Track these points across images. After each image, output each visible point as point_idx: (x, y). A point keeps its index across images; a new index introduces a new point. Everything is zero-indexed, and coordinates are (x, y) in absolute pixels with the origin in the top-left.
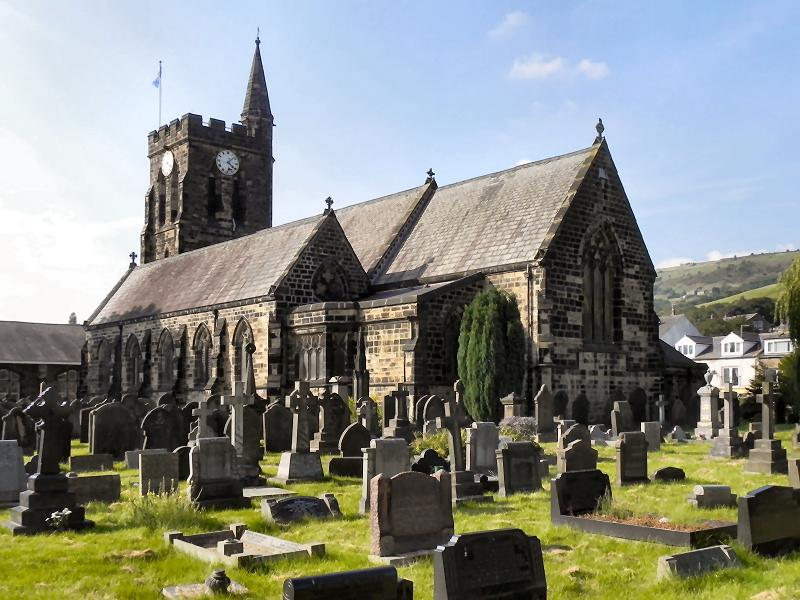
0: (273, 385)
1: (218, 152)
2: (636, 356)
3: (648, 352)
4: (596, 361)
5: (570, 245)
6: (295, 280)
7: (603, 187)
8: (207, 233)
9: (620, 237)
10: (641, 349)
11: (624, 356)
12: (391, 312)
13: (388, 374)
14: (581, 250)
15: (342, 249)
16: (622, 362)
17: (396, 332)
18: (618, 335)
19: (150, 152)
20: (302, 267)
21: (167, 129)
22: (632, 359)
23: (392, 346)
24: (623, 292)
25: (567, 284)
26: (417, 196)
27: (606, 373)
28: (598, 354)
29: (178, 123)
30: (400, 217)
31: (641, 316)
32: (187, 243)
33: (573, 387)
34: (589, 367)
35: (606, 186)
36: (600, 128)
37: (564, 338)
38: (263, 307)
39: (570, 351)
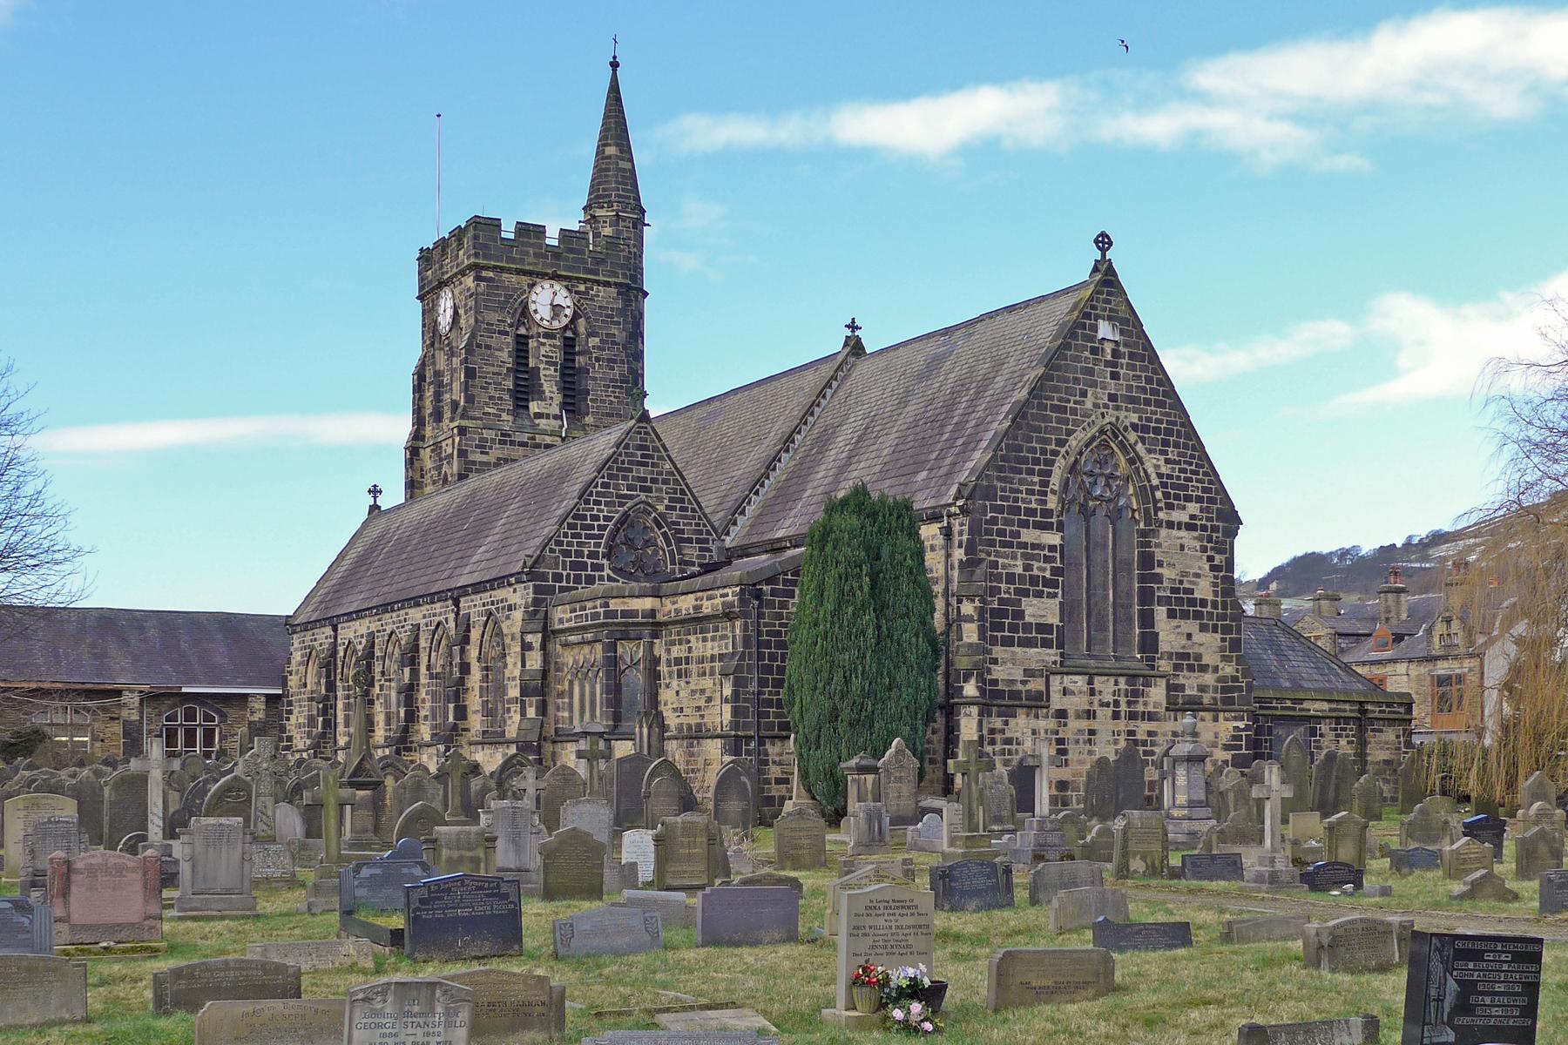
1: (532, 286)
2: (1190, 683)
3: (1221, 673)
4: (1092, 692)
6: (569, 544)
7: (1109, 357)
8: (512, 443)
9: (1149, 451)
10: (1204, 668)
11: (1163, 683)
12: (706, 603)
14: (1055, 481)
15: (665, 482)
16: (1157, 694)
17: (713, 639)
18: (1150, 643)
19: (421, 288)
20: (584, 518)
21: (442, 244)
22: (1182, 687)
24: (1158, 557)
25: (1024, 545)
26: (826, 371)
27: (1116, 716)
28: (1097, 679)
29: (458, 233)
31: (1203, 603)
32: (474, 463)
35: (1115, 353)
36: (1103, 242)
37: (1016, 649)
38: (518, 593)
39: (1029, 673)
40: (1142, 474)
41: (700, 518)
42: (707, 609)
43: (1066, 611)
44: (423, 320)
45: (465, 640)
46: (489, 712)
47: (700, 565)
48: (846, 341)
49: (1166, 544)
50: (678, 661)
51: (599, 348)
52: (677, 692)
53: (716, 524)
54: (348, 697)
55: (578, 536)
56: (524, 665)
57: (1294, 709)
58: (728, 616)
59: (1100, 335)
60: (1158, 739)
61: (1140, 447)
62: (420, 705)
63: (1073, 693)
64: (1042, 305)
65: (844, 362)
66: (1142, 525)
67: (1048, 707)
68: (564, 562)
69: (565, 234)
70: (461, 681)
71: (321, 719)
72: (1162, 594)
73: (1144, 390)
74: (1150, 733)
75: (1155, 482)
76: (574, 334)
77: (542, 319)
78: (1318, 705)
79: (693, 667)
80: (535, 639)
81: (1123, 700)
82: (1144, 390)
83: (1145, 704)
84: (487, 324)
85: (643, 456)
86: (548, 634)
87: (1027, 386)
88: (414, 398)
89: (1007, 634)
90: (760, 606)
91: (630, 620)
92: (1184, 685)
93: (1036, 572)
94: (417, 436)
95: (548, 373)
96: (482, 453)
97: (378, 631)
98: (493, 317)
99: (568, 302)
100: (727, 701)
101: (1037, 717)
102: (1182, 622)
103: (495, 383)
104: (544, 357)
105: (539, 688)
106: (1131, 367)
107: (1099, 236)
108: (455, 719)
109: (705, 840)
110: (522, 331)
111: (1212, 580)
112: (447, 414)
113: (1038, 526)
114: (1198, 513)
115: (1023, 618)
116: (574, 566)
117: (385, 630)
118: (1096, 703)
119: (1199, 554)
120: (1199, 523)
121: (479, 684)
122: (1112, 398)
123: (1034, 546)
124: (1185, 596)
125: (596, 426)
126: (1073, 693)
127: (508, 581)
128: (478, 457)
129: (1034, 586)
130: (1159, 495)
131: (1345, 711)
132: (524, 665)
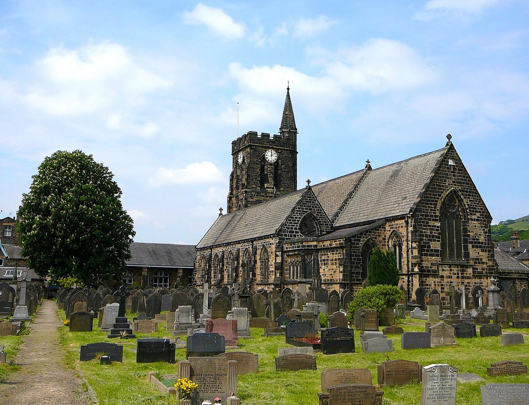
0: (276, 282)
2: (479, 267)
3: (488, 264)
5: (431, 204)
6: (289, 225)
8: (260, 196)
9: (465, 198)
10: (483, 263)
12: (333, 243)
13: (333, 277)
16: (470, 271)
17: (336, 254)
18: (467, 255)
21: (240, 139)
23: (334, 262)
25: (430, 226)
26: (360, 175)
27: (458, 277)
30: (351, 188)
31: (482, 243)
32: (249, 201)
33: (435, 285)
34: (446, 273)
35: (454, 169)
36: (449, 137)
37: (429, 257)
40: (463, 204)
41: (326, 218)
42: (334, 246)
43: (443, 245)
44: (233, 160)
45: (256, 253)
46: (263, 274)
47: (326, 232)
48: (366, 166)
50: (324, 260)
51: (284, 168)
52: (324, 270)
53: (330, 219)
54: (215, 270)
55: (292, 223)
56: (276, 261)
58: (342, 247)
59: (450, 164)
60: (471, 285)
62: (240, 272)
64: (430, 155)
65: (366, 172)
66: (463, 220)
67: (438, 275)
68: (287, 231)
69: (275, 136)
70: (254, 266)
71: (207, 276)
73: (462, 180)
74: (468, 283)
75: (467, 207)
76: (277, 164)
77: (269, 160)
79: (329, 262)
80: (279, 254)
81: (460, 272)
82: (462, 180)
83: (466, 274)
84: (253, 162)
85: (309, 200)
86: (283, 252)
87: (429, 179)
88: (230, 183)
90: (351, 244)
91: (310, 248)
93: (433, 234)
94: (231, 193)
96: (251, 198)
97: (226, 250)
98: (255, 160)
100: (341, 272)
102: (476, 249)
104: (268, 170)
105: (280, 267)
107: (448, 135)
108: (252, 277)
109: (376, 316)
110: (263, 164)
112: (241, 188)
113: (434, 220)
116: (291, 232)
117: (228, 250)
118: (452, 273)
121: (260, 266)
123: (433, 226)
127: (270, 236)
128: (250, 200)
129: (432, 238)
130: (468, 210)
132: (276, 261)
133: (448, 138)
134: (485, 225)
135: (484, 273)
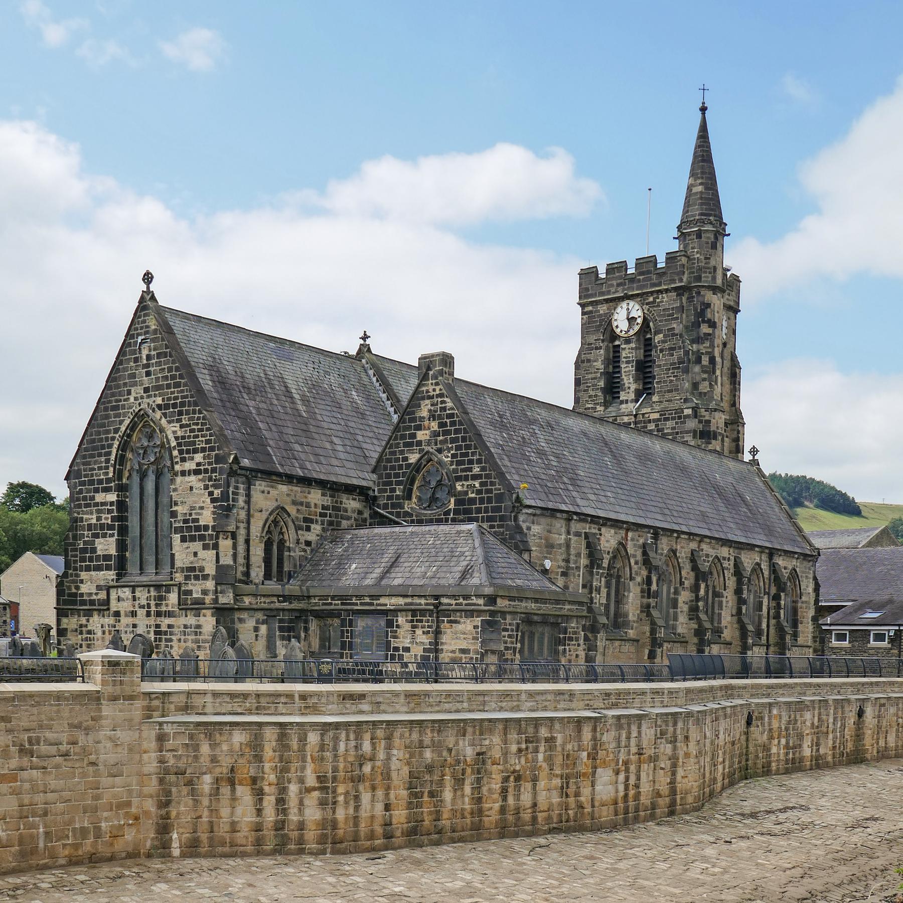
2: (196, 589)
7: (145, 362)
9: (169, 422)
22: (190, 592)
25: (96, 504)
27: (148, 614)
31: (206, 528)
34: (125, 607)
36: (148, 278)
37: (93, 573)
39: (99, 588)
49: (181, 488)
57: (372, 604)
60: (175, 630)
61: (164, 421)
63: (123, 600)
69: (671, 258)
72: (177, 525)
73: (166, 378)
74: (170, 626)
77: (621, 331)
78: (394, 600)
82: (166, 378)
83: (167, 605)
84: (588, 344)
89: (88, 563)
92: (192, 590)
93: (103, 521)
95: (627, 369)
99: (640, 313)
101: (104, 616)
102: (191, 544)
103: (593, 385)
106: (159, 364)
111: (212, 509)
114: (202, 461)
115: (96, 552)
119: (203, 491)
120: (202, 468)
122: (146, 390)
123: (103, 504)
124: (192, 525)
125: (660, 402)
126: (123, 600)
131: (420, 604)
133: (145, 282)
134: (215, 480)
135: (207, 601)
